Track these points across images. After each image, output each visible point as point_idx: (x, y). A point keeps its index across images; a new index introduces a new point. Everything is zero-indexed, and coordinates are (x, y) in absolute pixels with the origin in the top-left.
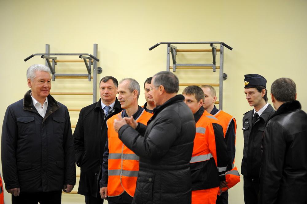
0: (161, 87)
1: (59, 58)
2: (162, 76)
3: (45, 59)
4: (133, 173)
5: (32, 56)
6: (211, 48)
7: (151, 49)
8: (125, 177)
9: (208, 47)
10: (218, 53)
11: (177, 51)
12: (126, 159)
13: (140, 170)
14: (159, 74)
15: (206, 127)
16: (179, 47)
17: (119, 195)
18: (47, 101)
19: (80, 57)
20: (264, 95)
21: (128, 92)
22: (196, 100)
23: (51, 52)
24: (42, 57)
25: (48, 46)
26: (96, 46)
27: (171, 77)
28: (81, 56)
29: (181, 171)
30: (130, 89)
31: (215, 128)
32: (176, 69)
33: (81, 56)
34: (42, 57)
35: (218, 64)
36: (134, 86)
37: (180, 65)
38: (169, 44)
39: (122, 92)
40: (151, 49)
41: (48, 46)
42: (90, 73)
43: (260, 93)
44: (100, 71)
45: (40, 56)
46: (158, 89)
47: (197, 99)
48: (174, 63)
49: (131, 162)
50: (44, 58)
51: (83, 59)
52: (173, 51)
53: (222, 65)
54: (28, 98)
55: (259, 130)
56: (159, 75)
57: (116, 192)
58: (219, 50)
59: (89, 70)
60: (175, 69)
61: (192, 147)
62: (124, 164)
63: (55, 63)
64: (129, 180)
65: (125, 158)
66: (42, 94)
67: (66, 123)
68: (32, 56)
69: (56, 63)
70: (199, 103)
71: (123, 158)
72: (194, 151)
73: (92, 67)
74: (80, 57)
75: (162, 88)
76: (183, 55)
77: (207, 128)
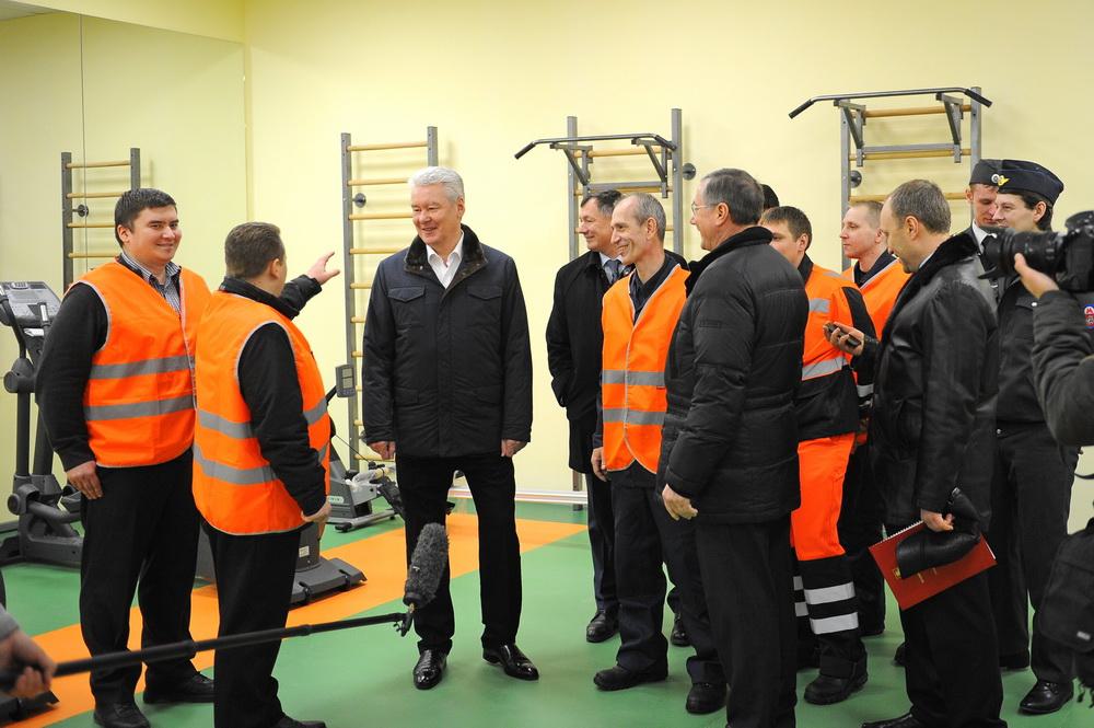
0: (720, 207)
1: (597, 146)
2: (726, 180)
3: (562, 151)
4: (650, 417)
5: (531, 146)
6: (941, 105)
7: (793, 115)
8: (632, 425)
9: (931, 101)
10: (967, 115)
11: (864, 115)
12: (635, 383)
13: (669, 411)
14: (717, 174)
15: (829, 296)
16: (871, 105)
17: (625, 468)
18: (458, 249)
19: (633, 143)
20: (1039, 216)
21: (633, 223)
22: (789, 235)
23: (581, 134)
24: (552, 147)
25: (573, 122)
26: (677, 114)
27: (746, 186)
28: (635, 140)
29: (758, 414)
30: (637, 217)
31: (848, 297)
32: (863, 159)
33: (635, 140)
34: (552, 147)
35: (965, 144)
36: (646, 211)
37: (874, 150)
38: (837, 101)
39: (620, 226)
40: (793, 115)
41: (573, 122)
42: (664, 179)
43: (1029, 211)
44: (690, 172)
45: (548, 145)
46: (713, 211)
47: (792, 233)
48: (859, 145)
49: (646, 391)
50: (557, 149)
51: (642, 147)
52: (854, 119)
53: (975, 144)
54: (418, 247)
55: (1018, 304)
56: (717, 180)
57: (617, 460)
58: (969, 109)
59: (663, 173)
60: (862, 160)
61: (800, 350)
62: (631, 397)
63: (589, 159)
64: (643, 435)
65: (633, 380)
66: (986, 216)
67: (504, 298)
68: (531, 146)
69: (591, 158)
70: (799, 242)
71: (629, 381)
72: (806, 356)
73: (670, 162)
74: (633, 143)
75: (723, 210)
76: (883, 125)
77: (834, 299)
